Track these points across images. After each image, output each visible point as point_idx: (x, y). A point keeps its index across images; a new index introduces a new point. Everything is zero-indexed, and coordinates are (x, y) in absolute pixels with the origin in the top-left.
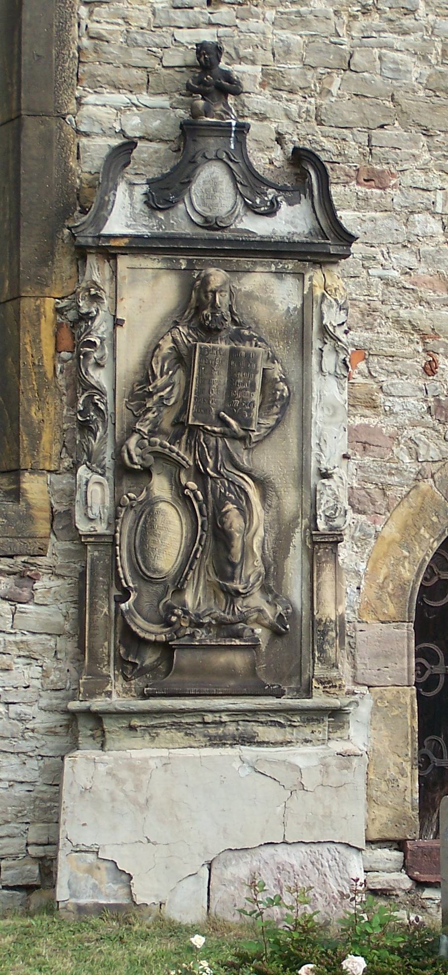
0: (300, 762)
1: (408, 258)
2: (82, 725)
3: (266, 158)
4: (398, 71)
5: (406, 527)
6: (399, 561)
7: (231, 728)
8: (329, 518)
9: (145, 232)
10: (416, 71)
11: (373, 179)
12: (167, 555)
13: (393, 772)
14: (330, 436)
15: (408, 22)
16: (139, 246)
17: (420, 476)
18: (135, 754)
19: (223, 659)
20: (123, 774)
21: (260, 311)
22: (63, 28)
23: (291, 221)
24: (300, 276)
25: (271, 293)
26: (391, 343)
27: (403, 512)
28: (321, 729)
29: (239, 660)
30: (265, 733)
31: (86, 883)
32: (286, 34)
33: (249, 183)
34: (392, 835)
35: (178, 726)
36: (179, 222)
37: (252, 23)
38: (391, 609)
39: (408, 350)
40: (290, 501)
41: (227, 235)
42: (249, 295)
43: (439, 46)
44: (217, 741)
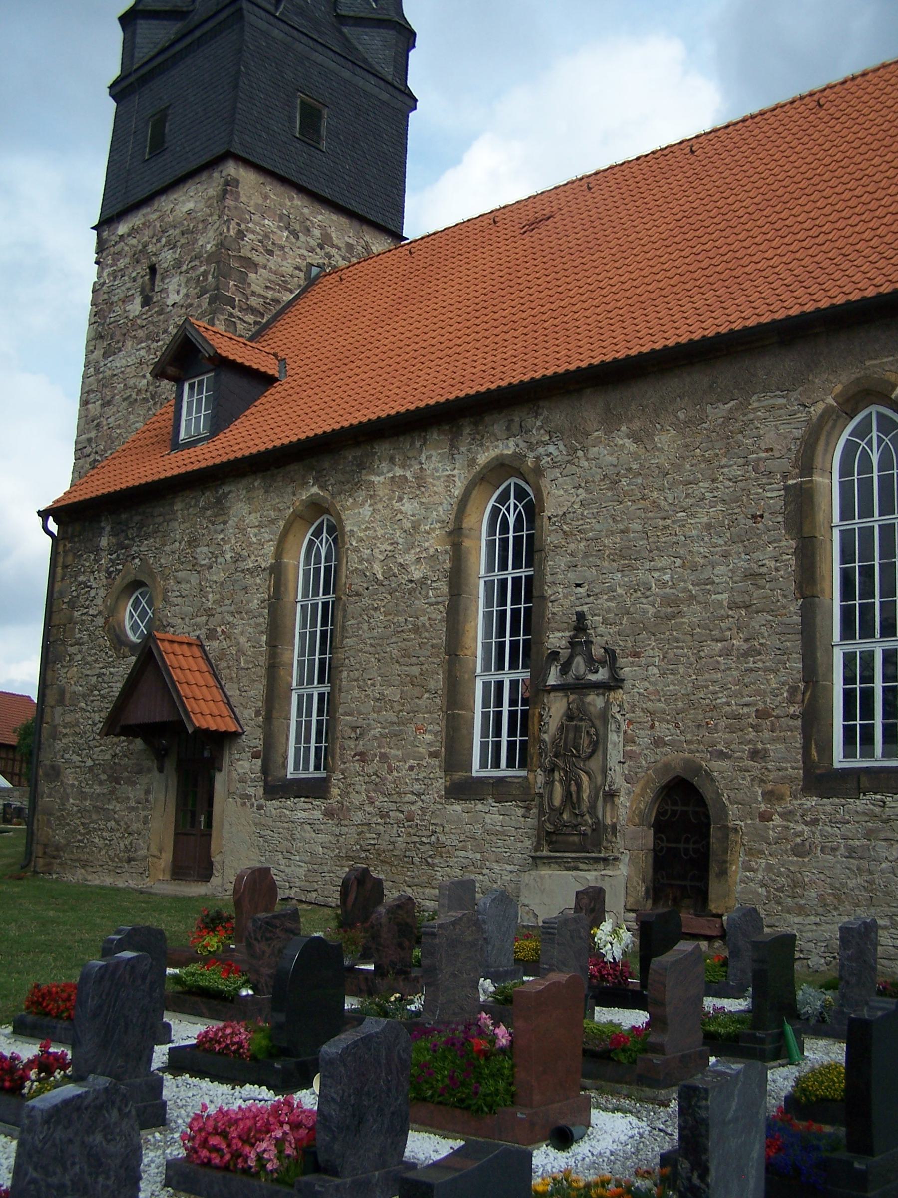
0: (589, 877)
1: (646, 684)
2: (536, 861)
3: (597, 652)
4: (645, 612)
5: (642, 789)
6: (640, 802)
7: (572, 864)
8: (610, 786)
9: (559, 683)
10: (651, 611)
11: (636, 655)
12: (557, 802)
13: (635, 884)
14: (614, 754)
15: (648, 593)
16: (555, 688)
17: (648, 769)
18: (543, 872)
19: (571, 838)
20: (538, 879)
21: (592, 709)
22: (544, 613)
23: (602, 675)
24: (604, 695)
25: (596, 701)
26: (639, 717)
27: (642, 782)
28: (601, 865)
29: (576, 839)
30: (582, 866)
31: (526, 917)
32: (608, 604)
33: (591, 662)
34: (634, 908)
35: (557, 863)
36: (570, 678)
37: (599, 602)
38: (637, 820)
39: (645, 720)
40: (599, 779)
41: (583, 682)
42: (589, 704)
43: (659, 601)
44: (568, 869)
